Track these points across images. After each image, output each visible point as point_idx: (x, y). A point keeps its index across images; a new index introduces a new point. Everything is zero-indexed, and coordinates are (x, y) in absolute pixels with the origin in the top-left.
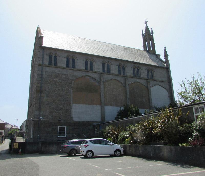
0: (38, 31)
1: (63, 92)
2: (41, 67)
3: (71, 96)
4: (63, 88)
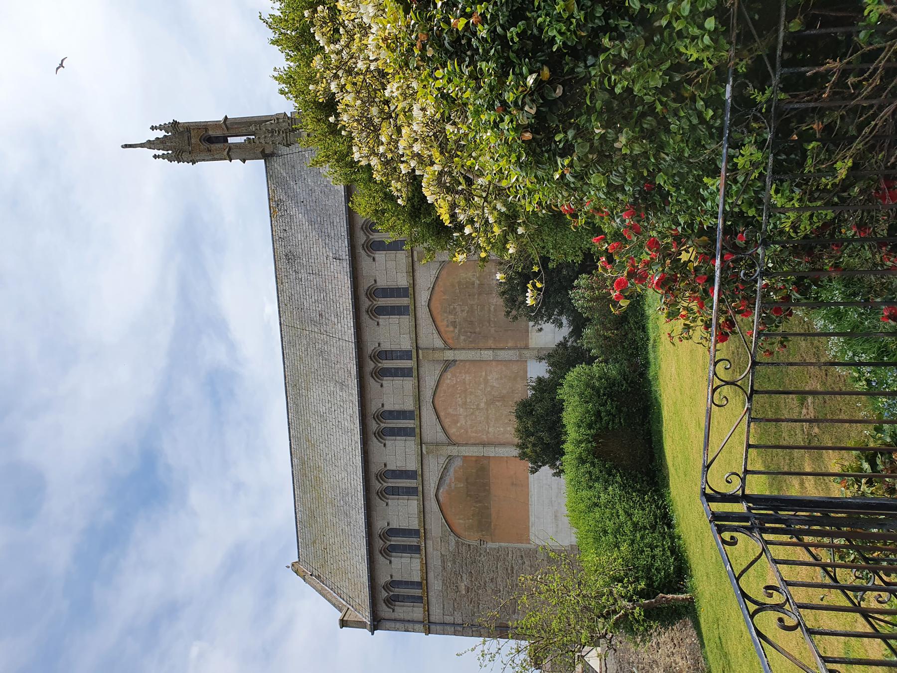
0: (122, 147)
1: (497, 568)
2: (433, 627)
3: (721, 155)
4: (485, 571)
